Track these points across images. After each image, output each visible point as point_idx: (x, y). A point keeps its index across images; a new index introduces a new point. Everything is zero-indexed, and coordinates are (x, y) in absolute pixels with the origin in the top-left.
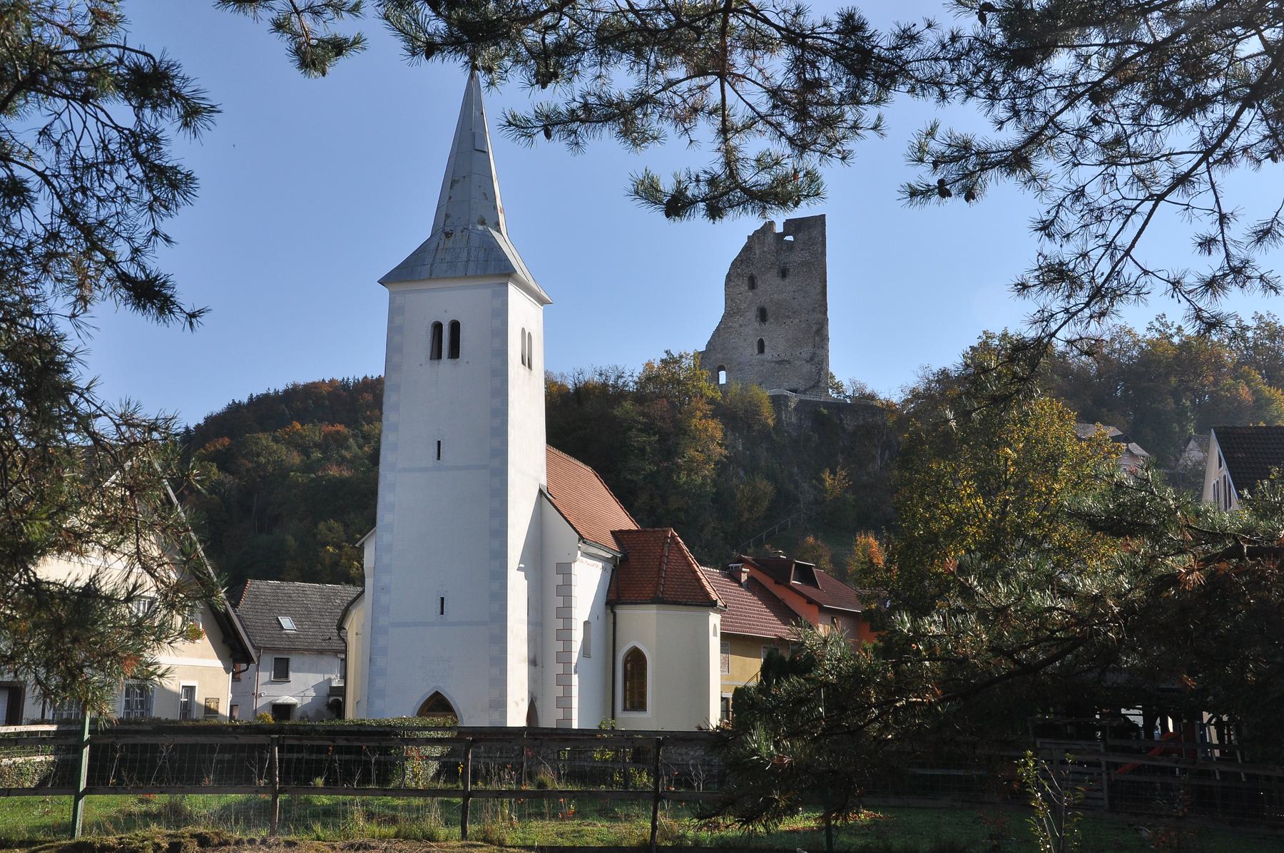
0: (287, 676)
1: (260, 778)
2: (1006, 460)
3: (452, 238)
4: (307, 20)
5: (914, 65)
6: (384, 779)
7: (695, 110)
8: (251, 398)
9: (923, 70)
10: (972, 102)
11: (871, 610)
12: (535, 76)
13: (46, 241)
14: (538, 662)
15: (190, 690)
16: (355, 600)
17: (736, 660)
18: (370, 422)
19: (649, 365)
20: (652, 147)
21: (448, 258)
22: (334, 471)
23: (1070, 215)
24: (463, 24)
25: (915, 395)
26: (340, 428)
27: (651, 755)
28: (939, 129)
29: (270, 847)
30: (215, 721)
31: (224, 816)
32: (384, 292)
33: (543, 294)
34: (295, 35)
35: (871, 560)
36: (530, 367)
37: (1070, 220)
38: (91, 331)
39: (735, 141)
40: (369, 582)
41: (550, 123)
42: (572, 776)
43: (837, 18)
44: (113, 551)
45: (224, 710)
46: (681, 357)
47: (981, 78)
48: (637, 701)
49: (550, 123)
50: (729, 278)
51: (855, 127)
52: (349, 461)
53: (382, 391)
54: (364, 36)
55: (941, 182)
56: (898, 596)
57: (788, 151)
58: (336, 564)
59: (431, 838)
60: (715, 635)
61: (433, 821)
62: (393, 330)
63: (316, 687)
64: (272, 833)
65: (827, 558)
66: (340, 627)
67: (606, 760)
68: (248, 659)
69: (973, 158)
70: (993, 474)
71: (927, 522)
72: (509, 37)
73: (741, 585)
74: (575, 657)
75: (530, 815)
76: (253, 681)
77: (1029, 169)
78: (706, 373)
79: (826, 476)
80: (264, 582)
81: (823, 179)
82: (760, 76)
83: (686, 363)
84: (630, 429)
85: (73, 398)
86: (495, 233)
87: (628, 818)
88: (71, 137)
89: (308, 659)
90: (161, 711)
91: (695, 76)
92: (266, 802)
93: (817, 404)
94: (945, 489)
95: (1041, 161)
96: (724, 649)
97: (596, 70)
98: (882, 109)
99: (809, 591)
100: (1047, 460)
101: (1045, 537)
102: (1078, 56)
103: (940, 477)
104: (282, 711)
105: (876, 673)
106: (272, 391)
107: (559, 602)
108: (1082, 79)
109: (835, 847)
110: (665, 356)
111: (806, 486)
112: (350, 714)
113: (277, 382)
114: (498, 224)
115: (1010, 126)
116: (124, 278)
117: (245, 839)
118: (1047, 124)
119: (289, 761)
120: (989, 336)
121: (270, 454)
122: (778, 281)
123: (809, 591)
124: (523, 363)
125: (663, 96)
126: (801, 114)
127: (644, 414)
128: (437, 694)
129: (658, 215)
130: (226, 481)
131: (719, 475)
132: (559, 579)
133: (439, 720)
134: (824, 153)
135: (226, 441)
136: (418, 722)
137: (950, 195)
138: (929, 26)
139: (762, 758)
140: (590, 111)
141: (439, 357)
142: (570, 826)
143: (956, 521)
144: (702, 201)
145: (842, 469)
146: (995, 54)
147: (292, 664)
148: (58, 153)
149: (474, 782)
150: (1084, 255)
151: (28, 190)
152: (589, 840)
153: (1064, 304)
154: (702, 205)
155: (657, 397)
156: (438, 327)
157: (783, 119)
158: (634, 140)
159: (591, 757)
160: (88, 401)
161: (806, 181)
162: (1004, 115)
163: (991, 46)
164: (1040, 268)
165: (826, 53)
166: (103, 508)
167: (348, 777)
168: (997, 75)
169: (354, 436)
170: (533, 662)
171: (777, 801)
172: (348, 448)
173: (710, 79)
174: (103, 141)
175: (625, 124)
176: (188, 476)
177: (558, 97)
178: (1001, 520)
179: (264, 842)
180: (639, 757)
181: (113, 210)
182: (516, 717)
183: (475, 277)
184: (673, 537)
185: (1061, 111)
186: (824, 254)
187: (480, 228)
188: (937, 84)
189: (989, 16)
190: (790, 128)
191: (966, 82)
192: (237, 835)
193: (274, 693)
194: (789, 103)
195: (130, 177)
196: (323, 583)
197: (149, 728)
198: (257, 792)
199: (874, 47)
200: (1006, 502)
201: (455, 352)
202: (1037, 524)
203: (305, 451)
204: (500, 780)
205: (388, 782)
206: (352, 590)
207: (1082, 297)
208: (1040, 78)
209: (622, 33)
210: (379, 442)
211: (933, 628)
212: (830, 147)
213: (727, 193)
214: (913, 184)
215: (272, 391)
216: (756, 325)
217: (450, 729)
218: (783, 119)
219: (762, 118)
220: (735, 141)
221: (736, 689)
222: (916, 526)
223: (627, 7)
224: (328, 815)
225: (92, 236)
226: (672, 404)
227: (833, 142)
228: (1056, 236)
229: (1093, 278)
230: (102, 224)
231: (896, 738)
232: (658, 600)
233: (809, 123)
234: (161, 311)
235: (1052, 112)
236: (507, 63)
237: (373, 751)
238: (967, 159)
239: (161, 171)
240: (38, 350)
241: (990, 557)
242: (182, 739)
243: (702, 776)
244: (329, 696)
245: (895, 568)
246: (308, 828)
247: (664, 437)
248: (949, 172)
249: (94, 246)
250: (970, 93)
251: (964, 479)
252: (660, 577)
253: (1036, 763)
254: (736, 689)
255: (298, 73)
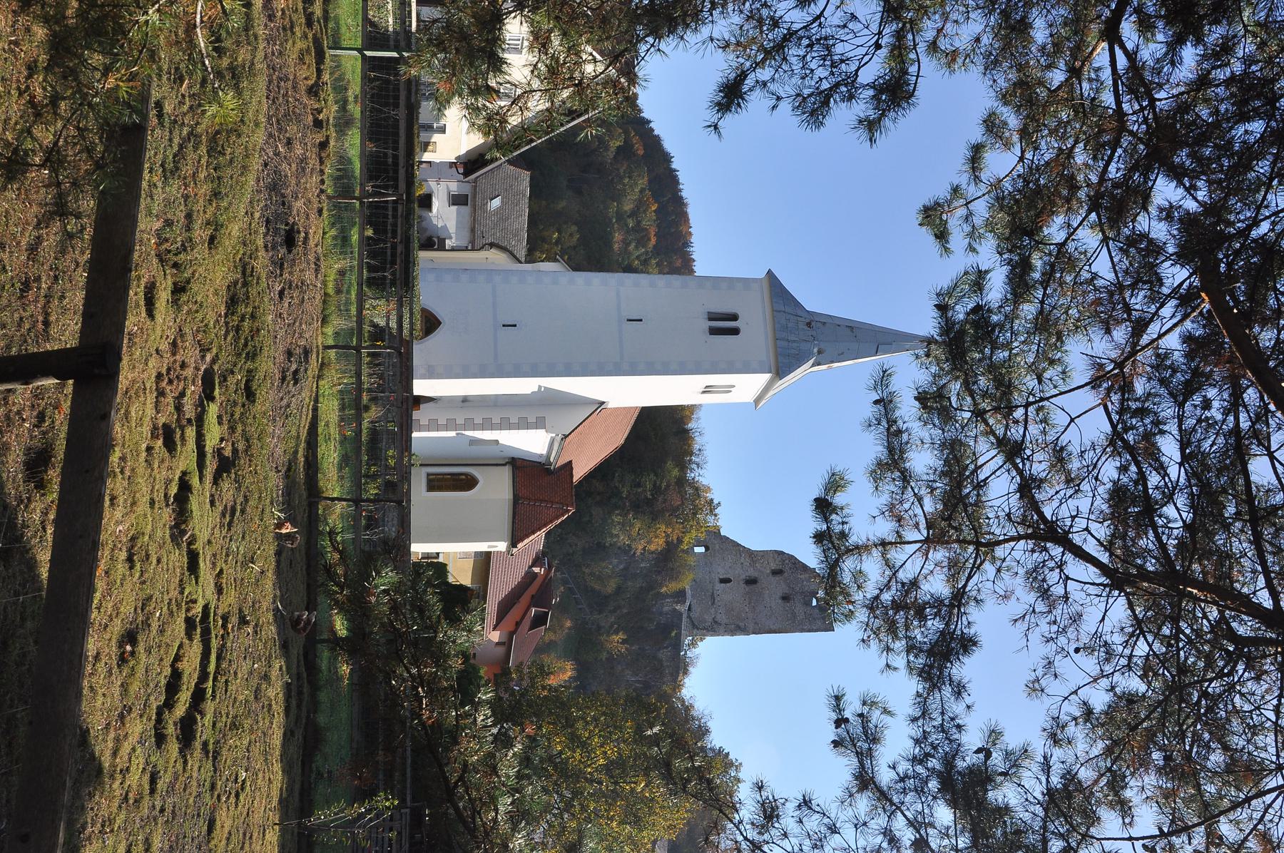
0: (453, 204)
1: (372, 187)
2: (635, 783)
3: (806, 328)
4: (962, 212)
5: (937, 695)
6: (371, 282)
7: (899, 519)
8: (675, 171)
9: (934, 704)
10: (910, 743)
11: (511, 673)
12: (924, 391)
13: (772, 18)
14: (466, 404)
15: (442, 130)
16: (515, 257)
17: (469, 564)
18: (658, 264)
19: (708, 489)
20: (870, 486)
21: (790, 325)
22: (618, 236)
23: (817, 822)
24: (962, 333)
25: (688, 708)
26: (653, 241)
27: (391, 496)
28: (889, 718)
29: (318, 196)
30: (418, 150)
31: (343, 160)
32: (762, 274)
33: (764, 401)
34: (949, 203)
35: (551, 673)
36: (704, 392)
37: (813, 823)
38: (701, 52)
39: (876, 553)
40: (529, 266)
41: (885, 404)
42: (374, 433)
43: (972, 631)
44: (532, 72)
45: (427, 157)
46: (716, 515)
47: (928, 749)
48: (435, 484)
49: (885, 404)
50: (782, 553)
51: (888, 649)
52: (626, 249)
53: (684, 274)
54: (951, 256)
55: (847, 720)
56: (522, 695)
57: (869, 596)
58: (544, 240)
59: (325, 321)
60: (489, 547)
61: (338, 323)
62: (731, 282)
63: (445, 227)
64: (329, 197)
65: (553, 638)
66: (492, 245)
67: (387, 460)
68: (466, 174)
69: (866, 746)
70: (623, 772)
71: (584, 719)
72: (953, 369)
73: (530, 567)
74: (469, 433)
75: (343, 399)
76: (450, 178)
77: (858, 792)
78: (702, 536)
79: (621, 636)
80: (528, 184)
81: (848, 625)
82: (927, 572)
83: (711, 519)
84: (656, 475)
85: (650, 40)
86: (811, 362)
87: (341, 478)
88: (851, 36)
89: (467, 220)
90: (426, 109)
91: (926, 519)
92: (354, 192)
93: (680, 628)
94: (610, 733)
95: (865, 801)
96: (477, 554)
97: (927, 439)
98: (903, 672)
99: (527, 623)
100: (635, 816)
101: (573, 815)
102: (948, 828)
103: (621, 728)
104: (426, 201)
105: (445, 671)
106: (681, 187)
107: (514, 420)
108: (930, 831)
109: (319, 646)
110: (716, 502)
111: (613, 619)
112: (423, 255)
113: (688, 190)
114: (819, 364)
115: (892, 775)
116: (742, 76)
117: (325, 177)
118: (894, 804)
119: (386, 209)
120: (738, 768)
121: (631, 186)
122: (780, 594)
123: (527, 623)
124: (707, 387)
125: (909, 493)
126: (897, 606)
127: (668, 486)
128: (440, 323)
129: (817, 492)
130: (609, 153)
131: (619, 548)
132: (532, 419)
133: (418, 325)
134: (867, 625)
135: (641, 152)
136: (417, 309)
137: (836, 728)
138: (968, 707)
139: (374, 579)
140: (896, 435)
141: (710, 319)
142: (334, 431)
143: (584, 742)
144: (828, 527)
145: (626, 649)
146: (949, 761)
147: (463, 208)
148: (839, 26)
149: (369, 354)
150: (785, 835)
151: (809, 5)
152: (323, 447)
153: (746, 820)
154: (825, 527)
155: (682, 496)
156: (734, 317)
157: (893, 591)
158: (875, 471)
159: (390, 448)
160: (648, 50)
161: (846, 612)
162: (901, 769)
163: (954, 757)
164: (775, 801)
165: (947, 624)
166: (565, 63)
167: (372, 255)
168: (933, 763)
169: (647, 253)
170: (465, 400)
171: (342, 593)
172: (637, 247)
173: (925, 533)
174: (848, 60)
175: (886, 464)
176: (590, 126)
177: (908, 410)
178: (586, 779)
179: (322, 191)
180: (390, 486)
181: (794, 68)
182: (421, 387)
183: (776, 346)
184: (568, 511)
185: (905, 816)
186: (802, 631)
187: (816, 350)
188: (923, 714)
189: (981, 756)
190: (886, 597)
191: (925, 738)
192: (328, 171)
193: (440, 194)
194: (906, 596)
195: (821, 79)
196: (528, 231)
197: (413, 100)
198: (361, 184)
199: (951, 663)
200: (600, 783)
201: (714, 331)
202: (584, 808)
203: (633, 214)
204: (370, 375)
205: (369, 286)
206: (522, 253)
207: (752, 834)
208: (930, 798)
209: (958, 460)
210: (642, 272)
211: (482, 718)
212: (872, 630)
213: (834, 547)
214: (845, 698)
215: (681, 187)
216: (744, 577)
217: (411, 334)
218: (893, 591)
219: (894, 574)
220: (876, 553)
221: (445, 565)
222: (579, 709)
223: (979, 464)
224: (344, 239)
225: (776, 51)
226: (677, 508)
227: (876, 633)
228: (798, 812)
229: (768, 843)
230: (785, 59)
231: (392, 687)
232: (516, 500)
233: (891, 612)
234: (718, 104)
235: (904, 808)
236: (934, 369)
237: (393, 274)
238: (865, 741)
239: (826, 103)
240: (685, 14)
241: (556, 771)
242: (402, 125)
243: (374, 537)
244: (438, 237)
245: (545, 693)
246: (333, 225)
247: (649, 503)
248: (855, 727)
249: (768, 53)
250: (917, 742)
251: (619, 749)
252: (535, 500)
253: (388, 808)
254: (446, 565)
255: (920, 206)
